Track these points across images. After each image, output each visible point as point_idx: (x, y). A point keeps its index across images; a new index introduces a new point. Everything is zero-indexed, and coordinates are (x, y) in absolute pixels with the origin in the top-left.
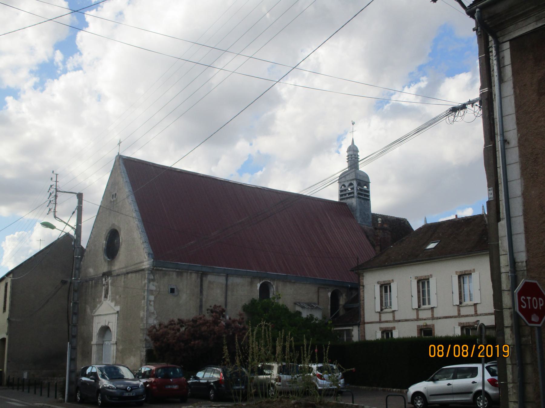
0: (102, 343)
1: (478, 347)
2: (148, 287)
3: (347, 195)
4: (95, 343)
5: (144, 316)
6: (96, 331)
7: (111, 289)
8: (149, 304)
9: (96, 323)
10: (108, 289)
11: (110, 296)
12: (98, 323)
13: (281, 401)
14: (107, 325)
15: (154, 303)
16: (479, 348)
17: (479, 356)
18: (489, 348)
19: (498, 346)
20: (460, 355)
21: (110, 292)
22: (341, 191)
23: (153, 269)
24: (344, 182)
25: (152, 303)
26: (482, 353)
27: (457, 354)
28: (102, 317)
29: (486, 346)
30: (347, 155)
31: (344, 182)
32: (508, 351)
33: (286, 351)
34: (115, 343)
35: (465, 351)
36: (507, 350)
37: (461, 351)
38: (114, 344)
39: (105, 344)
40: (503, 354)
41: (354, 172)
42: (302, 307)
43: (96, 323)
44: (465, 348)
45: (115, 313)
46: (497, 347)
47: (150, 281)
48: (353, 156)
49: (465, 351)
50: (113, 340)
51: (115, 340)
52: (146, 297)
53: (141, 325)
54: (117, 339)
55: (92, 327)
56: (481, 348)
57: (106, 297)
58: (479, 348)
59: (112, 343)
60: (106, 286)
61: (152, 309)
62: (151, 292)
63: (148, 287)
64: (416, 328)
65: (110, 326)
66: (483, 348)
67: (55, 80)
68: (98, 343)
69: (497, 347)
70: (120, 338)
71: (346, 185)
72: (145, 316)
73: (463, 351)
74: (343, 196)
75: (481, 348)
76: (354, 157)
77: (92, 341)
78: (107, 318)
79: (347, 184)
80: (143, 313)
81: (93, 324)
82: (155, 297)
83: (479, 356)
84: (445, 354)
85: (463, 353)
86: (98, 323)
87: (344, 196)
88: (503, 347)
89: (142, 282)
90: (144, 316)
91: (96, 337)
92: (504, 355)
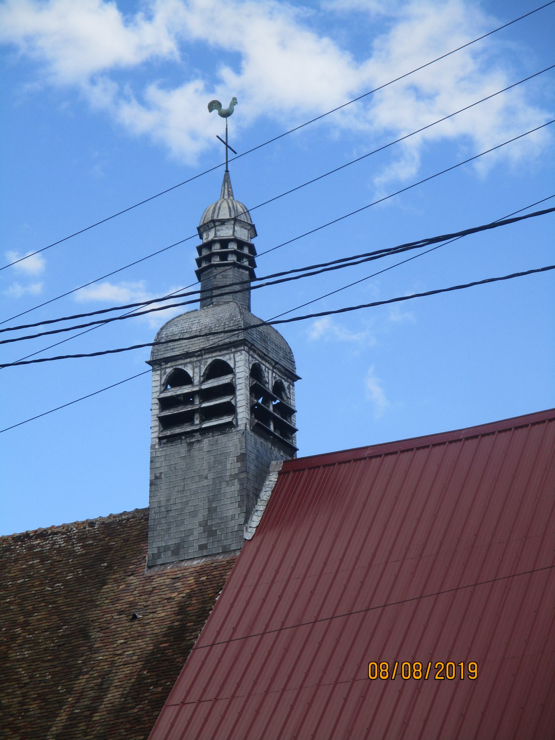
3: (197, 401)
13: (161, 473)
17: (437, 677)
19: (462, 664)
22: (165, 403)
26: (440, 673)
30: (298, 452)
32: (476, 671)
33: (203, 370)
36: (475, 669)
40: (470, 675)
41: (210, 227)
42: (4, 726)
46: (461, 666)
48: (233, 246)
58: (436, 667)
64: (197, 229)
66: (441, 667)
69: (461, 666)
75: (439, 668)
76: (234, 252)
83: (437, 677)
92: (470, 677)
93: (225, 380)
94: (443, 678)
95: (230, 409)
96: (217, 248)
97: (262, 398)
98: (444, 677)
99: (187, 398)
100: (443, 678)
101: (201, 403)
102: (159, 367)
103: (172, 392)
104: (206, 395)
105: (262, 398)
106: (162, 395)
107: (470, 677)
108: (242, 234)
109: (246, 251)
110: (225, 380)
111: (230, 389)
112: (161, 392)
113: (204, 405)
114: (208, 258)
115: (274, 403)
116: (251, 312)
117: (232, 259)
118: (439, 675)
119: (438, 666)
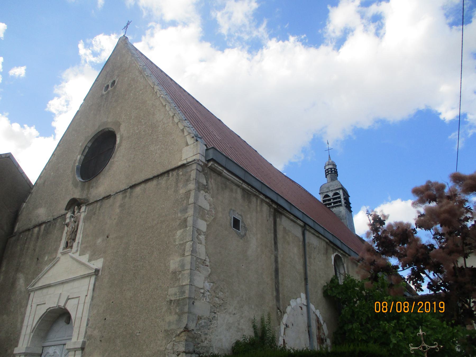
0: (40, 352)
1: (418, 304)
2: (196, 198)
4: (24, 351)
5: (183, 266)
6: (30, 322)
7: (85, 229)
8: (197, 238)
9: (34, 306)
10: (77, 231)
11: (78, 243)
12: (38, 305)
14: (62, 304)
15: (206, 238)
16: (418, 305)
17: (419, 311)
18: (427, 304)
19: (435, 303)
20: (402, 311)
21: (79, 236)
23: (206, 165)
24: (327, 192)
25: (202, 237)
27: (399, 310)
28: (51, 290)
29: (425, 303)
31: (327, 192)
32: (444, 307)
34: (79, 346)
35: (406, 307)
37: (403, 307)
38: (75, 350)
39: (48, 353)
43: (34, 306)
44: (406, 305)
45: (89, 276)
46: (434, 304)
47: (200, 187)
49: (406, 307)
50: (74, 339)
51: (81, 340)
52: (190, 221)
53: (172, 291)
54: (88, 337)
55: (23, 315)
56: (420, 304)
57: (68, 245)
58: (418, 305)
59: (72, 347)
60: (72, 225)
61: (201, 249)
62: (200, 211)
63: (196, 198)
65: (70, 308)
67: (63, 84)
68: (29, 351)
69: (434, 304)
70: (96, 333)
71: (329, 195)
72: (188, 267)
73: (405, 307)
74: (326, 202)
75: (420, 304)
76: (333, 171)
77: (16, 346)
78: (65, 291)
79: (331, 194)
80: (178, 259)
81: (25, 309)
82: (208, 225)
83: (419, 311)
84: (389, 310)
85: (404, 309)
86: (38, 305)
87: (327, 201)
88: (440, 304)
89: (176, 191)
90: (183, 266)
91: (27, 337)
92: (440, 311)
93: (339, 196)
94: (422, 312)
95: (340, 202)
96: (329, 170)
97: (421, 274)
98: (423, 311)
99: (330, 200)
100: (422, 312)
101: (334, 205)
102: (343, 264)
103: (325, 199)
104: (334, 199)
105: (421, 274)
106: (323, 200)
107: (440, 311)
108: (331, 166)
109: (336, 170)
110: (339, 196)
111: (339, 197)
112: (323, 199)
113: (334, 201)
114: (328, 172)
115: (447, 290)
116: (339, 178)
117: (333, 172)
118: (420, 310)
119: (419, 304)
